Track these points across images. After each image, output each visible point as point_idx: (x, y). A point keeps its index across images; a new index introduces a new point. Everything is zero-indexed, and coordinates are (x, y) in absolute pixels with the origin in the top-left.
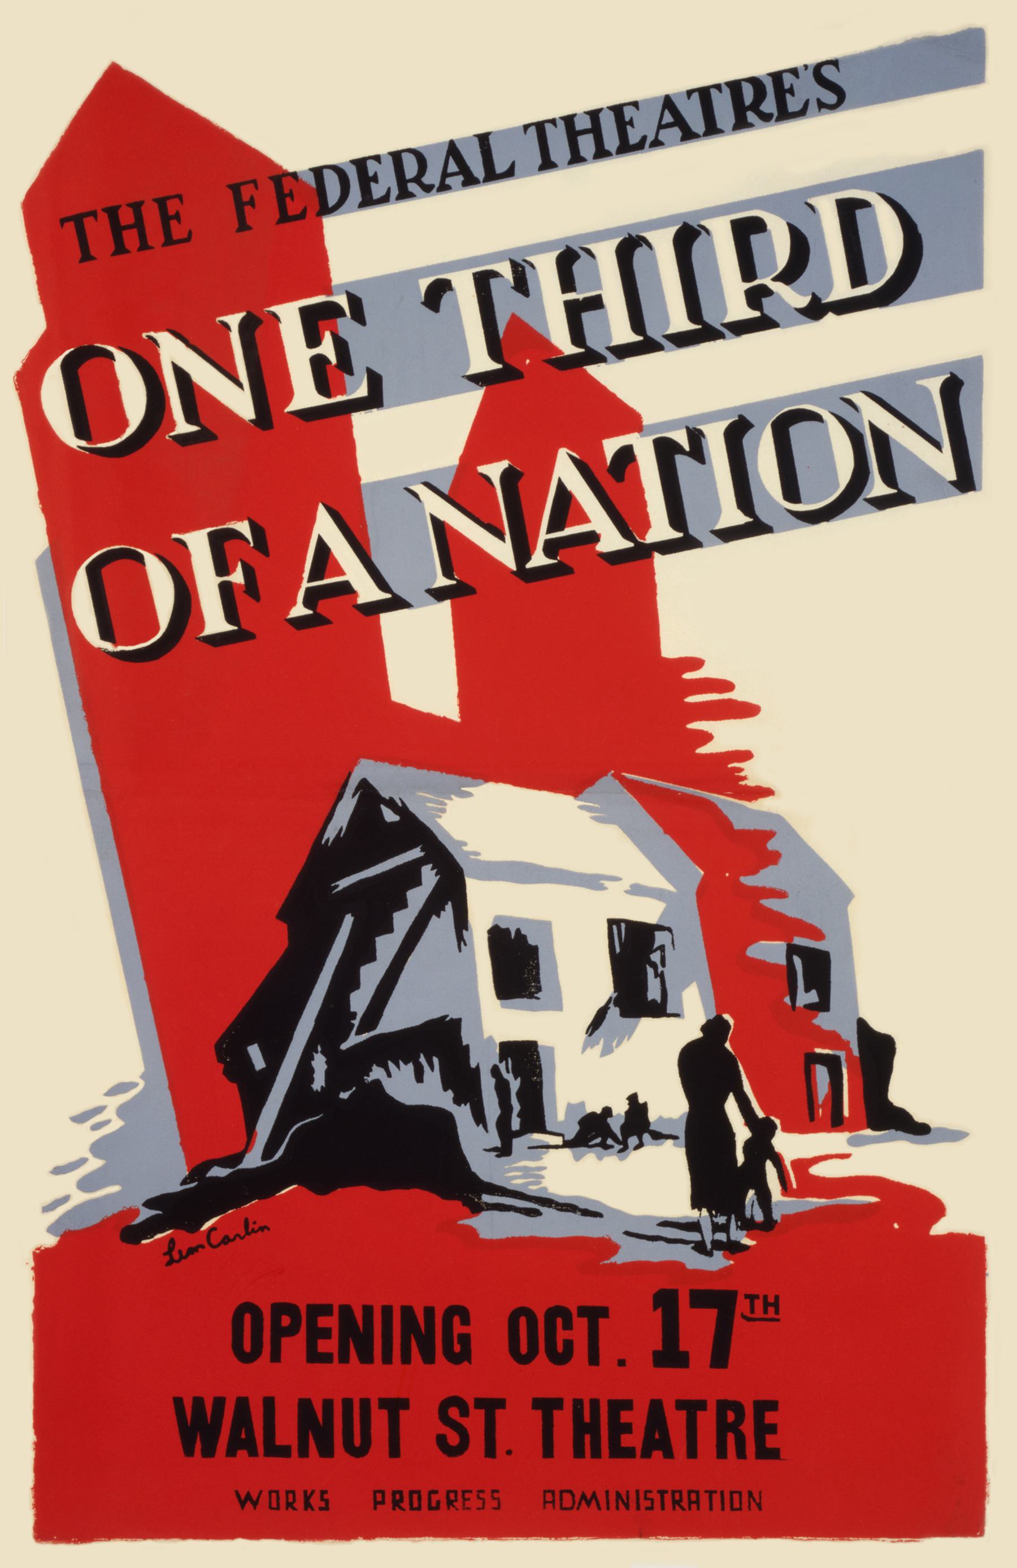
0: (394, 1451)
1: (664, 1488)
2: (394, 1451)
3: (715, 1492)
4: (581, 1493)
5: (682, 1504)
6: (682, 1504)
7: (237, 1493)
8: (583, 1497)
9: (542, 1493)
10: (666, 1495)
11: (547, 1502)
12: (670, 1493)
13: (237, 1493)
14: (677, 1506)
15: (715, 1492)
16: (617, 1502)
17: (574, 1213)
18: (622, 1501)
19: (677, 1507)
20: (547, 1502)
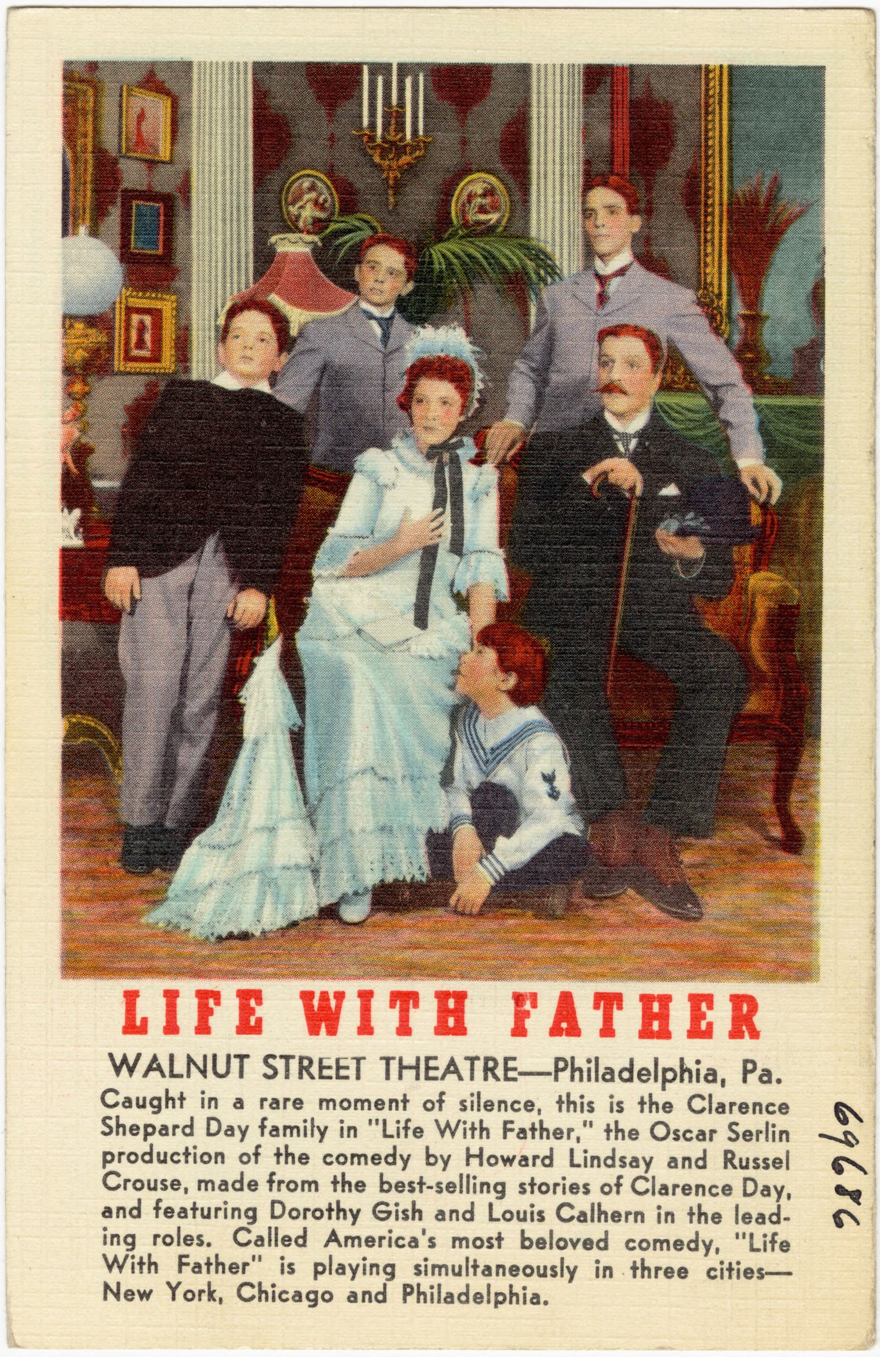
0: (241, 1075)
1: (390, 1054)
2: (241, 1075)
3: (393, 1058)
4: (124, 1270)
5: (497, 1071)
6: (497, 1071)
7: (111, 1055)
8: (676, 1131)
9: (742, 1182)
10: (291, 1061)
11: (407, 1067)
12: (297, 1058)
13: (111, 1055)
14: (304, 1073)
15: (393, 1058)
16: (205, 1065)
17: (808, 980)
18: (453, 515)
19: (729, 1165)
20: (407, 1067)
